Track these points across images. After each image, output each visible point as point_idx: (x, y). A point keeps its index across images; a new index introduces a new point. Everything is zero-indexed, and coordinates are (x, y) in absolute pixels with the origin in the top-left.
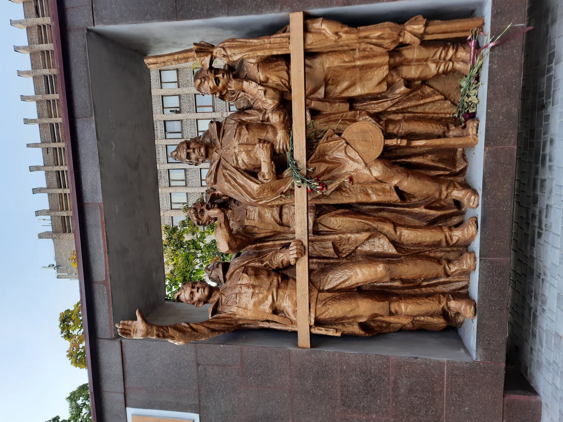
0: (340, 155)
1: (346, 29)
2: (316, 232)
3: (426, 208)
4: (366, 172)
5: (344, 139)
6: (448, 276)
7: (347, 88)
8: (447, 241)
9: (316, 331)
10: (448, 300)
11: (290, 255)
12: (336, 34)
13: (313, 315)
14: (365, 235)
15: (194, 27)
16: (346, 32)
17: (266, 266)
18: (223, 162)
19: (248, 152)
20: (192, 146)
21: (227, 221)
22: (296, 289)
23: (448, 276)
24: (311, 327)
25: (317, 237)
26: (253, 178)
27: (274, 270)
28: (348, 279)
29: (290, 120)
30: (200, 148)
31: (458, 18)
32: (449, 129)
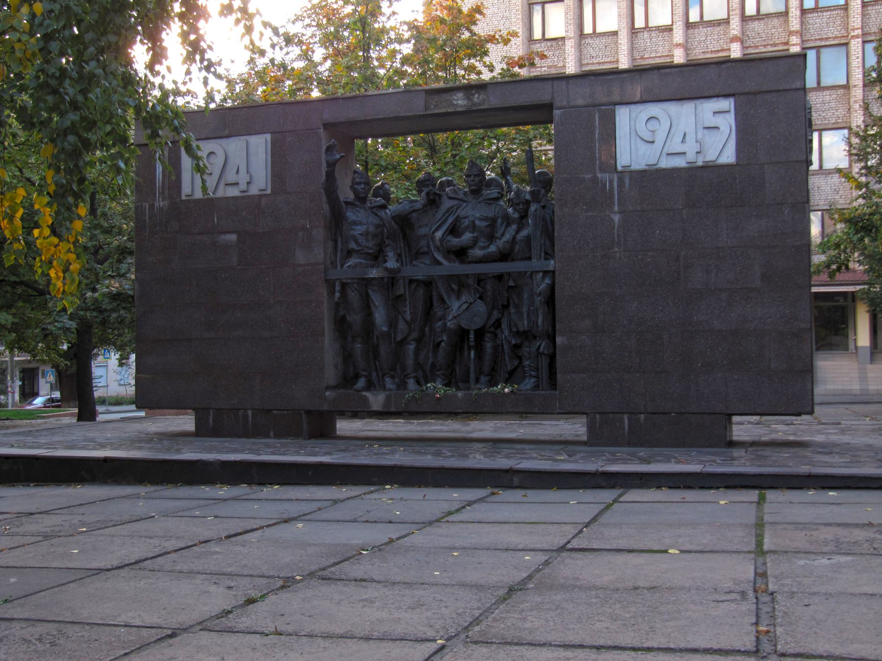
0: (464, 298)
1: (543, 300)
2: (411, 281)
3: (432, 363)
4: (450, 317)
5: (475, 301)
6: (383, 377)
7: (514, 302)
8: (406, 375)
9: (337, 284)
10: (366, 377)
11: (392, 264)
12: (540, 293)
13: (348, 281)
14: (408, 318)
15: (102, 446)
16: (541, 300)
17: (385, 242)
18: (465, 204)
19: (467, 227)
20: (477, 179)
21: (415, 211)
22: (326, 161)
23: (383, 377)
24: (340, 279)
25: (407, 282)
26: (448, 232)
27: (381, 248)
28: (376, 306)
29: (495, 261)
30: (475, 185)
31: (765, 475)
32: (486, 375)
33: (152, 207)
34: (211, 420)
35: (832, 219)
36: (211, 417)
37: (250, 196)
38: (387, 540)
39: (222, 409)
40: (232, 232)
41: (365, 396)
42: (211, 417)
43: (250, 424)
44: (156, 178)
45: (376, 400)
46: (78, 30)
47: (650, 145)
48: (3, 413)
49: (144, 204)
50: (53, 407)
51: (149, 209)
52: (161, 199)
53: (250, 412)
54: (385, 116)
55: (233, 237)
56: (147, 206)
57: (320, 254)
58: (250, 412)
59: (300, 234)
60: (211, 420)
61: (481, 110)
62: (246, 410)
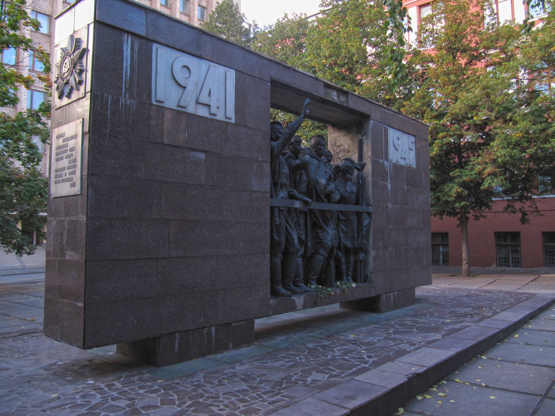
24: (278, 207)
33: (116, 101)
34: (176, 345)
35: (296, 382)
36: (177, 342)
37: (218, 121)
38: (500, 22)
39: (188, 331)
40: (201, 151)
41: (294, 300)
42: (177, 342)
43: (213, 340)
44: (122, 70)
45: (299, 300)
46: (452, 403)
47: (395, 150)
48: (4, 374)
49: (106, 95)
50: (497, 258)
51: (112, 103)
52: (128, 95)
53: (213, 329)
54: (304, 90)
55: (202, 156)
56: (110, 100)
57: (268, 184)
58: (213, 329)
59: (255, 165)
60: (176, 345)
61: (358, 226)
62: (210, 327)
